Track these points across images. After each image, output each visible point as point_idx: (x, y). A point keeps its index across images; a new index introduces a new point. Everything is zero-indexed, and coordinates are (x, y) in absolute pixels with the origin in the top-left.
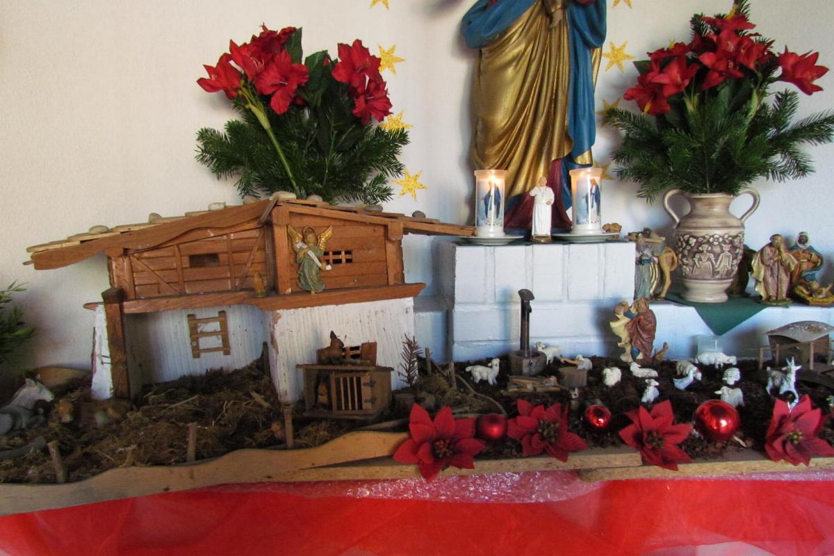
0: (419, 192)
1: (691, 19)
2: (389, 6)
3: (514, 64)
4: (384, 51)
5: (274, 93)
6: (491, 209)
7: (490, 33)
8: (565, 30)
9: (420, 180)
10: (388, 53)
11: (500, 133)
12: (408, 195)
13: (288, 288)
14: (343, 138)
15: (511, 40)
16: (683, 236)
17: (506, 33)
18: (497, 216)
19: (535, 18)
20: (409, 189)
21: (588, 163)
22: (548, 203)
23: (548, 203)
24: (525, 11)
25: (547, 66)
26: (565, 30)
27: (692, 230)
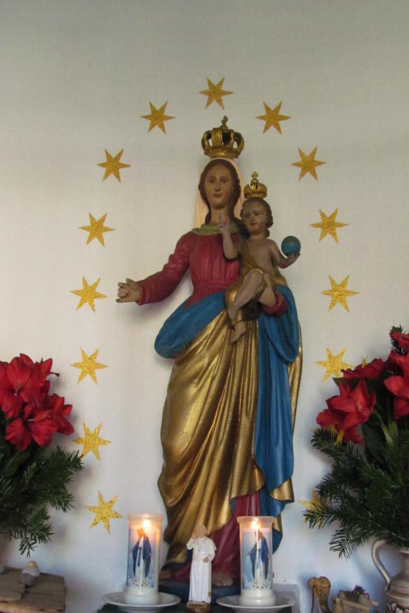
0: (113, 521)
1: (390, 332)
2: (95, 308)
3: (196, 381)
4: (86, 356)
5: (227, 314)
6: (139, 565)
7: (174, 345)
8: (253, 343)
9: (115, 508)
10: (90, 359)
11: (179, 461)
12: (101, 524)
13: (400, 440)
14: (11, 462)
15: (198, 349)
16: (391, 605)
17: (190, 344)
18: (146, 575)
19: (220, 329)
20: (102, 518)
21: (287, 498)
22: (206, 560)
23: (206, 560)
24: (211, 320)
25: (231, 384)
26: (253, 343)
27: (398, 598)
